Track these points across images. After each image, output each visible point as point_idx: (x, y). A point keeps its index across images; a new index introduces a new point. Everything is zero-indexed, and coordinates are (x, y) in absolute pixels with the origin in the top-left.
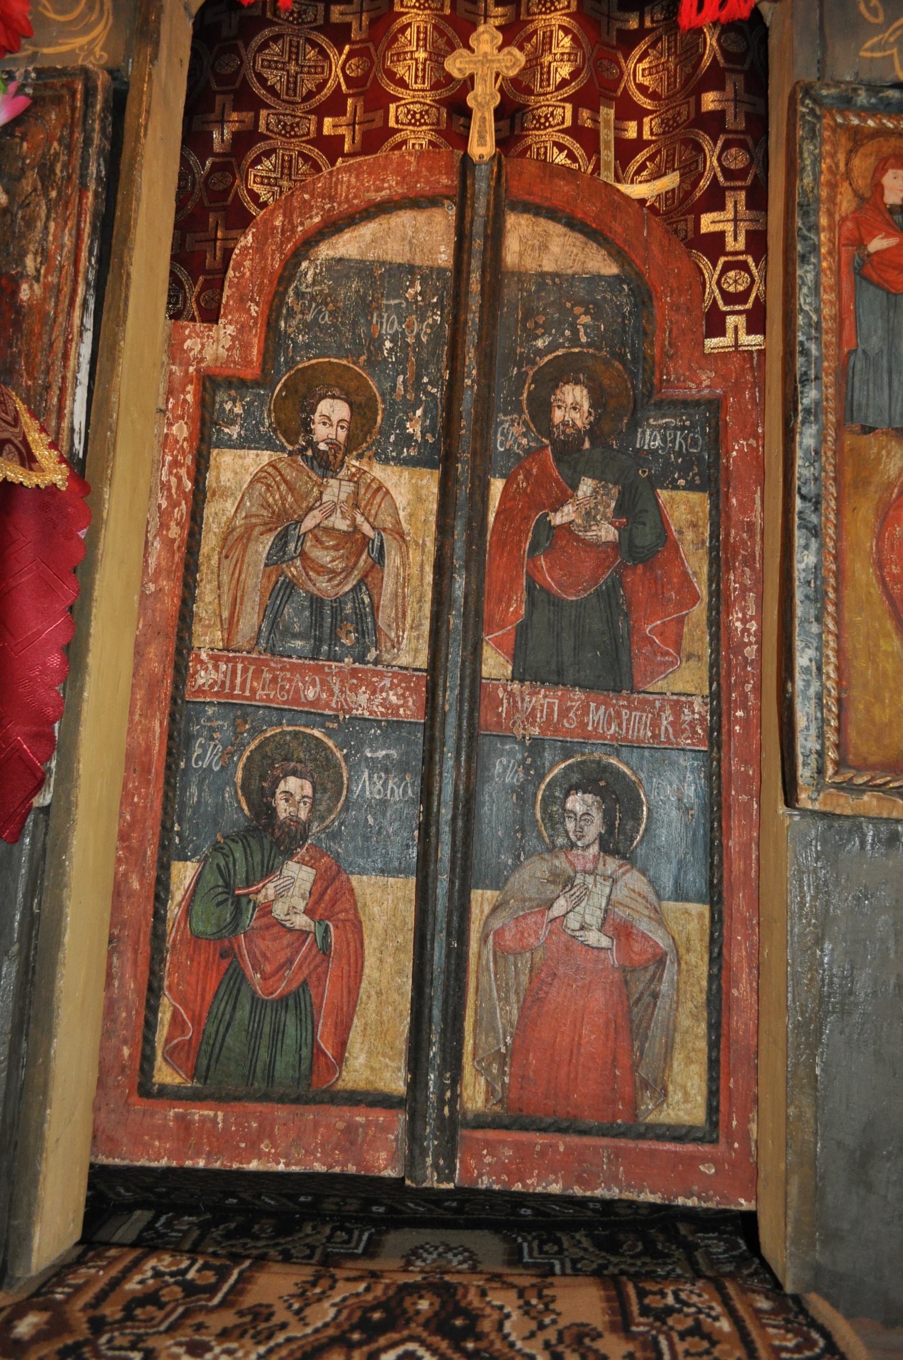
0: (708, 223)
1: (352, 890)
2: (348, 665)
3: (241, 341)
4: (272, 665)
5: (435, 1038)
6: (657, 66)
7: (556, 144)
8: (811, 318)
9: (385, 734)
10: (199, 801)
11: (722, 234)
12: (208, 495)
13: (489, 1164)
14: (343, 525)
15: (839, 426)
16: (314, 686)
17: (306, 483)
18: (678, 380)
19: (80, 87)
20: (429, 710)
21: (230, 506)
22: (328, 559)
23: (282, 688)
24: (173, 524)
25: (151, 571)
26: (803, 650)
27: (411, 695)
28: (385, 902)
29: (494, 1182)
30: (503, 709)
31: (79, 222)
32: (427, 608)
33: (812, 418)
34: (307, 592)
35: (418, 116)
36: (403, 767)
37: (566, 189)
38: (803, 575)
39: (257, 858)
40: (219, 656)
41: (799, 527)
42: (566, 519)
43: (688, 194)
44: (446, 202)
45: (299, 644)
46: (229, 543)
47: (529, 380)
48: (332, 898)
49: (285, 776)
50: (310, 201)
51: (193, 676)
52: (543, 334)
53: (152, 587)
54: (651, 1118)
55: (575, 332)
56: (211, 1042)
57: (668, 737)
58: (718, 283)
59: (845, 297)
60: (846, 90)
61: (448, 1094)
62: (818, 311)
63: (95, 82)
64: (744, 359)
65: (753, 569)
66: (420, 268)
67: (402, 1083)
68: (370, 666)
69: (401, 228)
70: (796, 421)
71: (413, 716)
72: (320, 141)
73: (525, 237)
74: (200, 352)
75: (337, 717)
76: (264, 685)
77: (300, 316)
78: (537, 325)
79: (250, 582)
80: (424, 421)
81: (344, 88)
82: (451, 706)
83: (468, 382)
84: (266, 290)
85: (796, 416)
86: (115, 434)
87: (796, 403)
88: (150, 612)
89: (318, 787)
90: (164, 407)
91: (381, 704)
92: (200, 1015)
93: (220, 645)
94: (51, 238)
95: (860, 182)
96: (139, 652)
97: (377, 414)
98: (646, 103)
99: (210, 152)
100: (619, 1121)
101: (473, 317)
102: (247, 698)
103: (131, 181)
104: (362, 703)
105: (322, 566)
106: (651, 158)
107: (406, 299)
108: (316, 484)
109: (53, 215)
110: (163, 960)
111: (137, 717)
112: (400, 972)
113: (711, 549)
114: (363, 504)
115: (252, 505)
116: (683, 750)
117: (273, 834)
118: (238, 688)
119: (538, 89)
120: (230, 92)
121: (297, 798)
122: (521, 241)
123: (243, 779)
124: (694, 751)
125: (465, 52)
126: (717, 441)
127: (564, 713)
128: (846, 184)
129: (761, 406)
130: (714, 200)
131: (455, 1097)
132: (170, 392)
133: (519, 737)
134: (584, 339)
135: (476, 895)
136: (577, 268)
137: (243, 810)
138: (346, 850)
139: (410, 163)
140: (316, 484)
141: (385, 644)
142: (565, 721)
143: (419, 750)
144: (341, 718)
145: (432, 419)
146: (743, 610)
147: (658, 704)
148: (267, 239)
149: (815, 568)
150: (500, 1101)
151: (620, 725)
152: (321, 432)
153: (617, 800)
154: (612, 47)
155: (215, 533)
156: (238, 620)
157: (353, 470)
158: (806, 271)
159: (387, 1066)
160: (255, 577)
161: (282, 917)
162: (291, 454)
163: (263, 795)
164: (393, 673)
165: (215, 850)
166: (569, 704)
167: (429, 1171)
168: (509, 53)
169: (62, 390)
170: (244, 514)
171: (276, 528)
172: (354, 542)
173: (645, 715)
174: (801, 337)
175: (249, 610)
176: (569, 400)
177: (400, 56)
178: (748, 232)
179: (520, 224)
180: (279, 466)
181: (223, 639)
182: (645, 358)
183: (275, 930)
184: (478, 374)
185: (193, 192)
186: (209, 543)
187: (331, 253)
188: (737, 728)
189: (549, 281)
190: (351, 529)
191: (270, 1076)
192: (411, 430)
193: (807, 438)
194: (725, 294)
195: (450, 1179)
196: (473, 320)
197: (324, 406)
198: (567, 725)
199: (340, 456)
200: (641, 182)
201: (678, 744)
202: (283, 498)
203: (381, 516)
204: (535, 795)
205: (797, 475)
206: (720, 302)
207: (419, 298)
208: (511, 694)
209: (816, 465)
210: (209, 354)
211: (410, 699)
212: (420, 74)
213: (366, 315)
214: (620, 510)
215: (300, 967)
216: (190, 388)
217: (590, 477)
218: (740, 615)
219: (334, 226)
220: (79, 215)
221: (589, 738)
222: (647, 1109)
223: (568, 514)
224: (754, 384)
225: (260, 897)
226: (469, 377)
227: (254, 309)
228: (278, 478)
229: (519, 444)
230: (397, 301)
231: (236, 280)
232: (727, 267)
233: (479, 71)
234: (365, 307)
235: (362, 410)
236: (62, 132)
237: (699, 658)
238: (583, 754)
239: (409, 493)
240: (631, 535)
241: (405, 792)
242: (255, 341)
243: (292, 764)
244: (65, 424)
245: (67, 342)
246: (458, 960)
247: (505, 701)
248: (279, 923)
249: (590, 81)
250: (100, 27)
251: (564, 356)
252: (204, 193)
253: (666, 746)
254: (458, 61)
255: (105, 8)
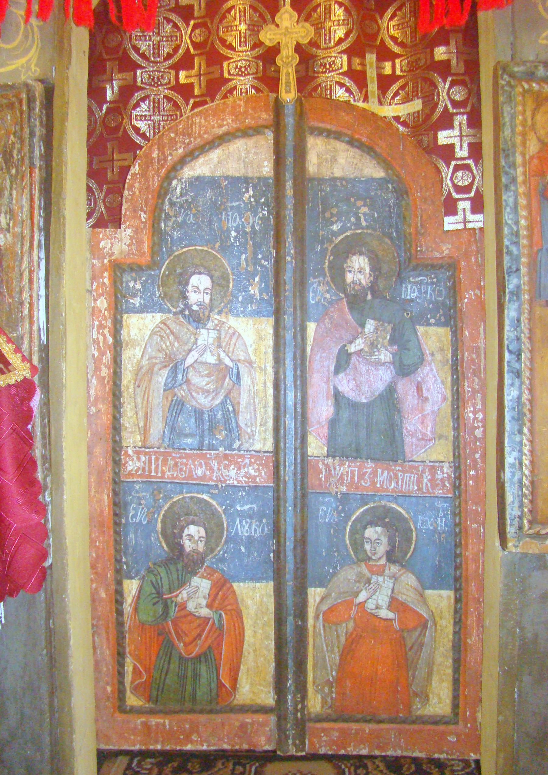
0: (444, 137)
1: (234, 592)
2: (222, 452)
3: (136, 240)
4: (174, 455)
5: (290, 676)
6: (403, 23)
7: (337, 83)
8: (512, 229)
9: (248, 494)
10: (136, 543)
11: (452, 146)
12: (124, 345)
13: (325, 741)
14: (211, 359)
15: (531, 302)
16: (201, 467)
17: (187, 333)
18: (428, 250)
19: (24, 96)
20: (275, 480)
21: (138, 352)
22: (204, 383)
23: (181, 469)
24: (103, 367)
25: (92, 399)
26: (510, 453)
27: (263, 469)
28: (256, 597)
29: (328, 750)
30: (322, 476)
31: (31, 189)
32: (270, 411)
33: (515, 298)
34: (192, 406)
35: (243, 69)
36: (260, 516)
37: (346, 118)
38: (511, 403)
39: (175, 576)
40: (140, 452)
41: (508, 372)
42: (358, 348)
43: (428, 117)
44: (266, 131)
45: (189, 440)
46: (139, 377)
47: (329, 254)
48: (222, 594)
49: (188, 525)
50: (175, 138)
51: (124, 465)
52: (336, 221)
53: (94, 409)
54: (419, 713)
55: (358, 219)
56: (158, 682)
57: (427, 489)
58: (451, 179)
59: (534, 213)
60: (530, 67)
61: (300, 706)
62: (517, 223)
63: (34, 92)
64: (470, 235)
65: (480, 378)
66: (252, 178)
67: (271, 700)
68: (236, 452)
69: (237, 151)
70: (505, 299)
71: (265, 482)
72: (179, 88)
73: (321, 153)
74: (111, 249)
75: (217, 486)
76: (169, 469)
77: (174, 219)
78: (332, 215)
79: (155, 402)
80: (261, 285)
81: (192, 50)
82: (289, 477)
83: (288, 259)
84: (151, 202)
85: (505, 296)
86: (64, 326)
87: (504, 288)
88: (94, 426)
89: (209, 531)
90: (90, 289)
91: (245, 476)
92: (150, 668)
93: (140, 444)
94: (14, 202)
95: (541, 131)
96: (90, 452)
97: (229, 283)
98: (396, 49)
99: (106, 101)
100: (401, 715)
101: (289, 213)
102: (159, 478)
103: (61, 152)
104: (233, 476)
105: (200, 388)
106: (402, 88)
107: (244, 201)
108: (192, 333)
109: (14, 186)
110: (124, 638)
111: (93, 493)
112: (267, 638)
113: (452, 365)
114: (224, 344)
115: (152, 351)
116: (437, 497)
117: (183, 561)
118: (153, 471)
119: (323, 46)
120: (117, 59)
121: (196, 538)
122: (318, 155)
123: (162, 528)
124: (444, 497)
125: (273, 27)
126: (455, 291)
127: (362, 476)
128: (533, 134)
129: (481, 266)
130: (446, 122)
131: (304, 707)
132: (94, 278)
133: (334, 493)
134: (364, 224)
135: (311, 591)
136: (357, 174)
137: (163, 547)
138: (229, 568)
139: (240, 106)
140: (192, 333)
141: (245, 437)
142: (362, 481)
143: (270, 503)
144: (220, 486)
145: (266, 283)
146: (474, 406)
147: (421, 468)
148: (148, 167)
149: (518, 398)
150: (330, 707)
151: (397, 483)
152: (193, 298)
153: (396, 530)
154: (373, 11)
155: (130, 371)
156: (150, 428)
157: (216, 322)
158: (509, 197)
159: (262, 691)
160: (158, 398)
161: (193, 610)
162: (175, 314)
163: (175, 537)
164: (251, 455)
165: (149, 572)
166: (364, 470)
167: (290, 747)
168: (303, 27)
169: (31, 304)
170: (147, 357)
171: (169, 365)
172: (221, 371)
173: (413, 476)
174: (506, 242)
175: (156, 421)
176: (356, 266)
177: (229, 28)
178: (470, 145)
179: (317, 145)
180: (168, 323)
181: (141, 441)
182: (405, 236)
183: (189, 618)
184: (296, 253)
185: (95, 128)
186: (127, 378)
187: (191, 173)
188: (471, 482)
189: (339, 184)
190: (217, 362)
191: (194, 699)
192: (252, 292)
193: (511, 312)
194: (455, 186)
195: (303, 750)
196: (289, 215)
197: (194, 280)
198: (363, 484)
199: (207, 314)
200: (396, 104)
201: (434, 493)
202: (172, 345)
203: (236, 352)
204: (345, 528)
205: (506, 337)
206: (449, 106)
207: (252, 200)
208: (327, 466)
209: (518, 329)
210: (116, 250)
211: (263, 472)
212: (243, 39)
213: (217, 215)
214: (393, 341)
215: (207, 637)
216: (106, 274)
217: (372, 319)
218: (472, 409)
219: (191, 156)
220: (31, 184)
221: (378, 491)
222: (417, 708)
223: (359, 345)
224: (478, 251)
225: (179, 599)
226: (289, 255)
227: (143, 216)
228: (168, 331)
229: (325, 298)
230: (237, 203)
231: (130, 197)
232: (457, 168)
233: (284, 41)
234: (217, 209)
235: (220, 283)
236: (15, 128)
237: (447, 438)
238: (374, 502)
239: (252, 334)
240: (400, 358)
241: (263, 530)
242: (146, 238)
243: (191, 517)
244: (35, 328)
245: (31, 272)
246: (301, 633)
247: (324, 470)
248: (191, 614)
249: (358, 36)
250: (33, 50)
251: (352, 235)
252: (104, 130)
253: (427, 495)
254: (268, 34)
255: (35, 36)
